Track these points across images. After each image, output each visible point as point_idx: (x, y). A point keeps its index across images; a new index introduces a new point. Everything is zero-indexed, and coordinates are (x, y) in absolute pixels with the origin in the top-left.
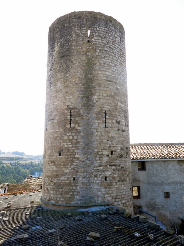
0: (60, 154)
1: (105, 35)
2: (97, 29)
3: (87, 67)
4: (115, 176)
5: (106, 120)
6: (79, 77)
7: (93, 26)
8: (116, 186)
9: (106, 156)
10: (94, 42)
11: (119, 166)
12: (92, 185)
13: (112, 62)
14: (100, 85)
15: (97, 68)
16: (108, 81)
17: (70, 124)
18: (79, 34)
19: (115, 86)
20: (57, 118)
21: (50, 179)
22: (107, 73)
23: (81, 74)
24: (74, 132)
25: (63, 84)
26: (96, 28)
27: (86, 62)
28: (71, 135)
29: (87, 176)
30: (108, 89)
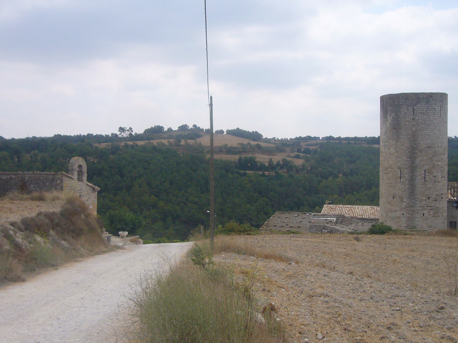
0: (393, 198)
1: (426, 111)
4: (430, 213)
5: (425, 176)
6: (406, 146)
7: (417, 105)
8: (430, 220)
11: (434, 207)
15: (419, 139)
17: (401, 178)
20: (391, 173)
21: (387, 213)
25: (395, 150)
26: (419, 107)
29: (411, 213)
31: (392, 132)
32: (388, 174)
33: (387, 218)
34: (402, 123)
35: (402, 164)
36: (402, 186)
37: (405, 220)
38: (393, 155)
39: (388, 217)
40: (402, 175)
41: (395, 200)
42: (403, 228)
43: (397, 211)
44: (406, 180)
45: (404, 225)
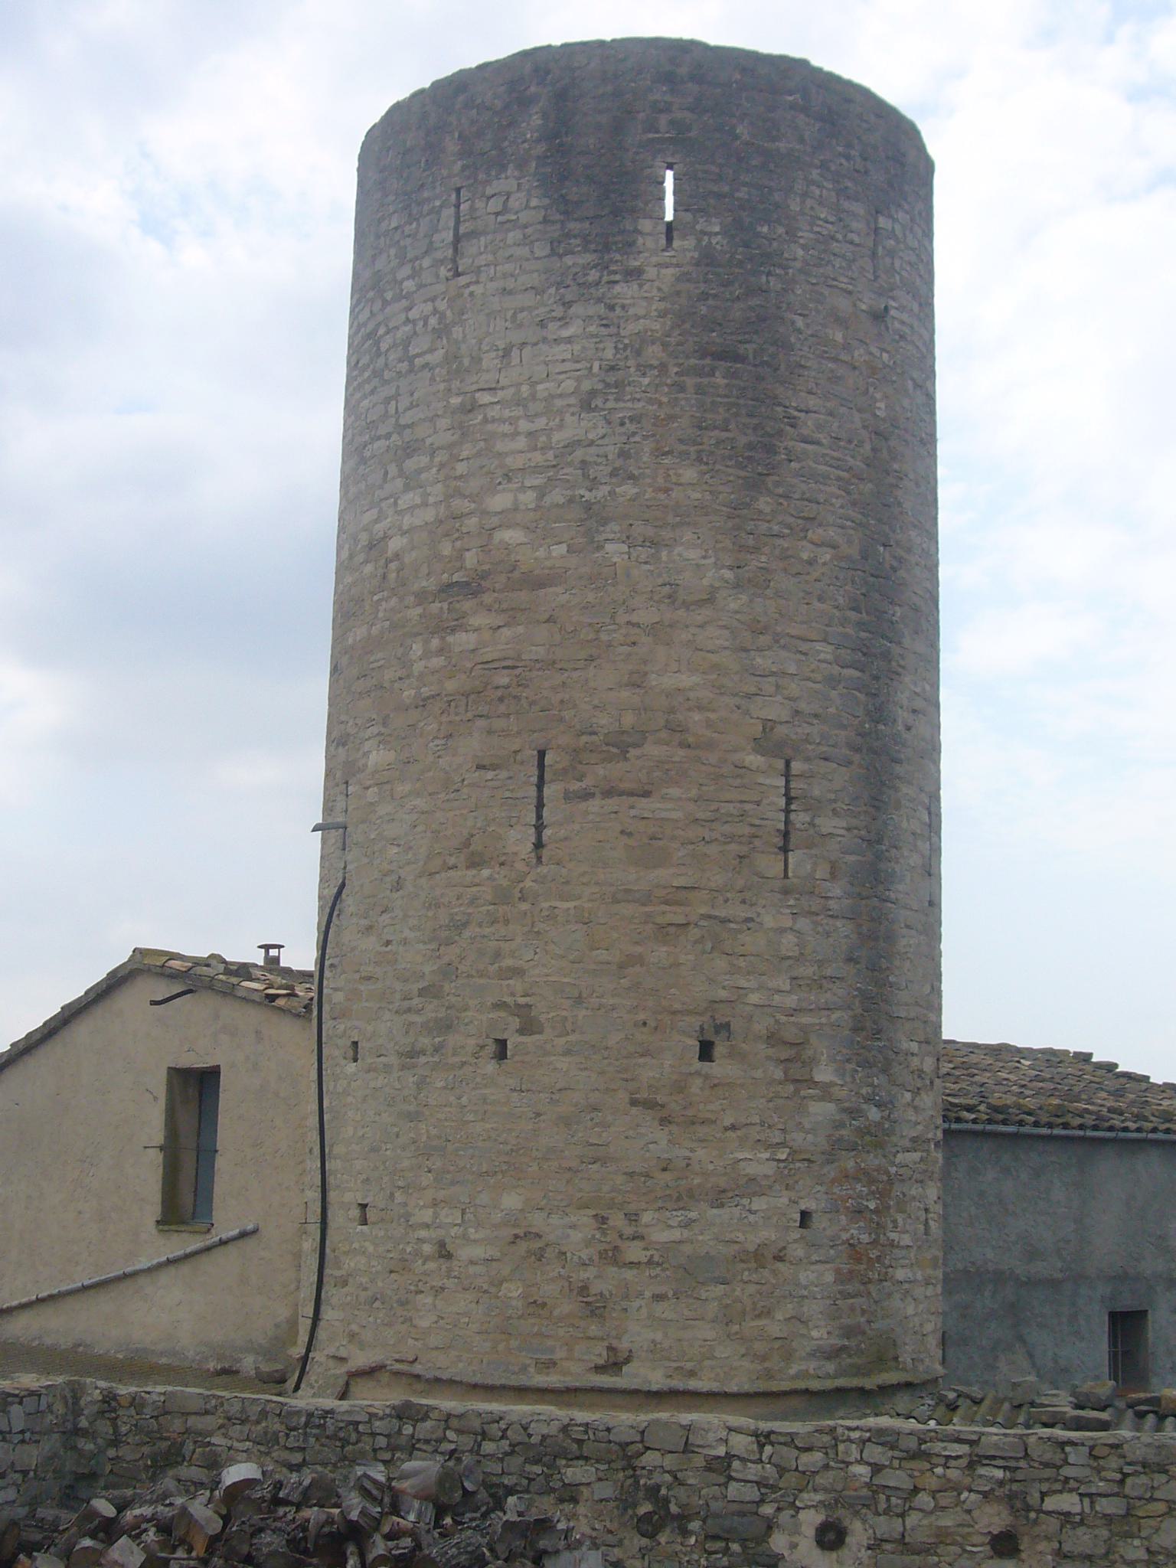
0: (706, 1052)
17: (785, 850)
18: (833, 238)
21: (617, 1220)
23: (842, 527)
31: (700, 390)
32: (646, 794)
33: (629, 1274)
34: (800, 323)
35: (802, 706)
36: (803, 924)
37: (829, 1277)
38: (706, 613)
39: (634, 1252)
40: (800, 818)
41: (721, 1068)
42: (812, 1366)
43: (753, 1187)
44: (833, 876)
45: (820, 1334)
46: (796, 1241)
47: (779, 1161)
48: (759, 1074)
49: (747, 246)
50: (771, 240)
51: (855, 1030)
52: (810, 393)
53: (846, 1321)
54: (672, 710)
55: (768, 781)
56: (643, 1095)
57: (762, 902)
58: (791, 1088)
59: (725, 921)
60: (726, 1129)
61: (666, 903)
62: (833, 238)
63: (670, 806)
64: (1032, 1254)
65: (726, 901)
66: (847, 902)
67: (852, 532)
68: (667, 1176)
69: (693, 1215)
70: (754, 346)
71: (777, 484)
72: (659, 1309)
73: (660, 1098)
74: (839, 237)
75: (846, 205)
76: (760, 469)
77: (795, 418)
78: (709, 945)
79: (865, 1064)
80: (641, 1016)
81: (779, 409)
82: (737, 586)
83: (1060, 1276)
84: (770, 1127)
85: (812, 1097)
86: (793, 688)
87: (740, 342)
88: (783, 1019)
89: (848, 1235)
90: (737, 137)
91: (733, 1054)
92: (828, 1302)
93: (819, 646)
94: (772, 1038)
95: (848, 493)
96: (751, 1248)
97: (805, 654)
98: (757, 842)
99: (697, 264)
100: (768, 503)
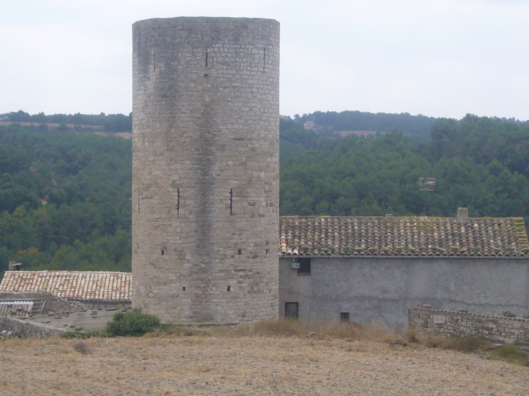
0: (163, 252)
2: (219, 50)
3: (203, 120)
5: (231, 204)
6: (190, 137)
7: (214, 46)
8: (243, 300)
9: (230, 257)
10: (214, 75)
11: (251, 271)
12: (208, 298)
13: (245, 104)
14: (222, 148)
16: (238, 139)
17: (178, 209)
18: (191, 60)
19: (249, 146)
21: (148, 288)
22: (236, 126)
23: (194, 132)
24: (184, 222)
26: (219, 48)
27: (202, 110)
28: (179, 226)
29: (203, 285)
30: (237, 153)
31: (160, 105)
32: (152, 198)
33: (150, 299)
34: (181, 84)
35: (182, 176)
37: (189, 301)
40: (181, 201)
41: (165, 257)
43: (172, 282)
44: (190, 213)
46: (181, 293)
47: (177, 276)
48: (172, 258)
49: (169, 68)
50: (174, 66)
51: (197, 247)
52: (184, 101)
53: (194, 310)
54: (156, 179)
55: (174, 194)
56: (152, 262)
57: (173, 220)
58: (180, 260)
59: (165, 225)
60: (166, 270)
61: (155, 222)
62: (191, 60)
63: (155, 201)
64: (385, 292)
65: (166, 221)
66: (195, 219)
67: (196, 132)
68: (156, 279)
69: (160, 287)
70: (170, 93)
71: (175, 125)
72: (155, 306)
73: (154, 263)
74: (193, 59)
75: (195, 50)
76: (172, 122)
77: (180, 108)
78: (162, 231)
79: (199, 254)
80: (151, 246)
81: (176, 107)
82: (167, 150)
83: (398, 298)
84: (175, 269)
85: (185, 262)
86: (179, 172)
87: (167, 92)
88: (178, 246)
89: (195, 292)
90: (167, 41)
91: (167, 253)
92: (190, 306)
93: (186, 162)
94: (175, 250)
95: (195, 123)
96: (172, 294)
97: (183, 164)
98: (172, 208)
99: (159, 75)
100: (173, 130)
